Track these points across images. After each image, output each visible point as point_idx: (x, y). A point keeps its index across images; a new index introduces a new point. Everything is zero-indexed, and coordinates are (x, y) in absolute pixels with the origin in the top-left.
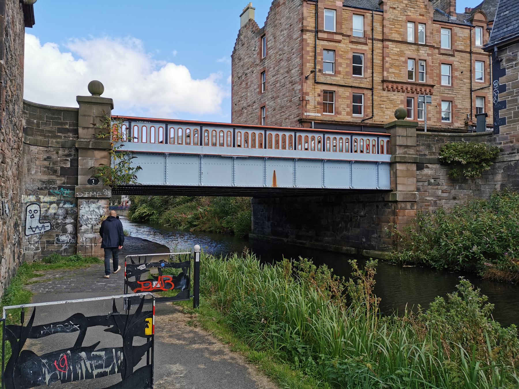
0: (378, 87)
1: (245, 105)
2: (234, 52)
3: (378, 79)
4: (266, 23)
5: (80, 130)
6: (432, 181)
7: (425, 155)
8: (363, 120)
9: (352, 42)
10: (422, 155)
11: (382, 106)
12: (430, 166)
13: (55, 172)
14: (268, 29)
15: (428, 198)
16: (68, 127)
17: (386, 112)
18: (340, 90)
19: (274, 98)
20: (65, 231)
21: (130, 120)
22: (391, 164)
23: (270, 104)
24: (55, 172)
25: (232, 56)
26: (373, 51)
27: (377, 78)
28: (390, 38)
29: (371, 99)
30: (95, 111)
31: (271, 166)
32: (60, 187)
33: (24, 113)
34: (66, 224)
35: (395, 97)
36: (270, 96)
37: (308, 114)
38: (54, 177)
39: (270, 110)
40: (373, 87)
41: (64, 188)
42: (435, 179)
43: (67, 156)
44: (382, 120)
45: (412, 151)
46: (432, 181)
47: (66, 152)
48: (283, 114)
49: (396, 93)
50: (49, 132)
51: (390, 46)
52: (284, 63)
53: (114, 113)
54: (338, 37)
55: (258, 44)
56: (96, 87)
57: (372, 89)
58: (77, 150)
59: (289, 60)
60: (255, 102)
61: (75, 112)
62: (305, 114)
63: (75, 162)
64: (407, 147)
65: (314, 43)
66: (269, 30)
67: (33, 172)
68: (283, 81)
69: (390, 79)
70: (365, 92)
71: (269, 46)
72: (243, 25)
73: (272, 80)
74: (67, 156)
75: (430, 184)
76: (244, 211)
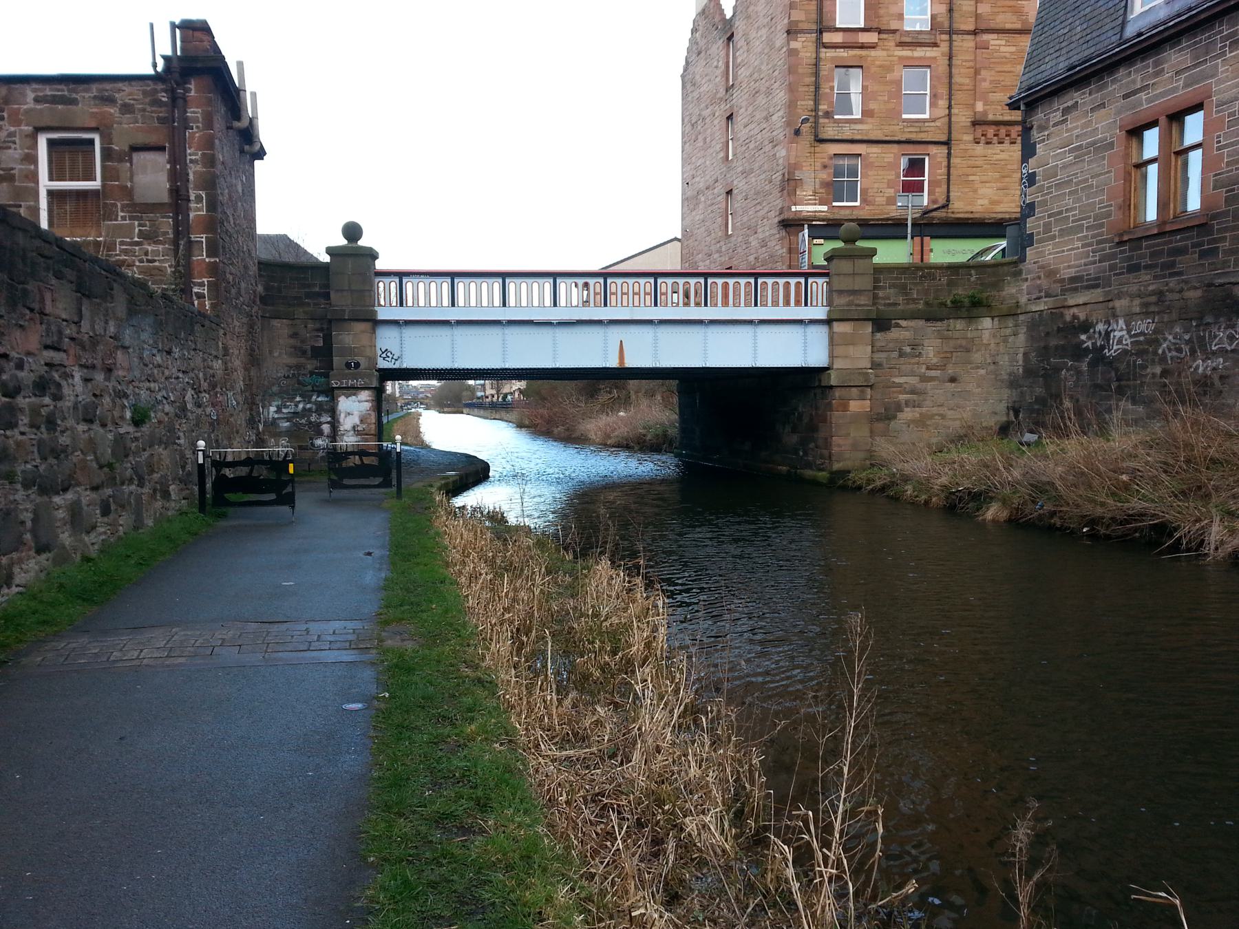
0: (964, 138)
1: (701, 185)
2: (685, 70)
3: (964, 119)
4: (735, 8)
5: (332, 295)
6: (908, 349)
7: (895, 304)
8: (925, 213)
9: (901, 44)
10: (890, 305)
11: (971, 178)
12: (903, 323)
13: (304, 353)
14: (737, 23)
15: (897, 380)
16: (317, 289)
17: (981, 191)
18: (875, 149)
19: (746, 173)
20: (320, 433)
21: (401, 275)
22: (828, 322)
23: (740, 185)
24: (304, 353)
25: (683, 76)
26: (950, 58)
27: (962, 117)
28: (993, 26)
29: (945, 163)
30: (350, 263)
31: (616, 334)
32: (312, 373)
33: (260, 276)
34: (321, 423)
35: (1003, 156)
36: (740, 169)
37: (799, 208)
38: (302, 360)
39: (739, 198)
40: (949, 139)
41: (317, 374)
42: (914, 346)
43: (317, 330)
44: (969, 208)
45: (863, 300)
46: (908, 349)
47: (318, 326)
48: (759, 207)
49: (1006, 146)
50: (296, 298)
51: (992, 42)
52: (761, 100)
53: (380, 265)
54: (872, 38)
55: (723, 53)
56: (352, 231)
57: (947, 143)
58: (330, 321)
59: (769, 92)
60: (716, 181)
61: (324, 267)
62: (793, 208)
63: (328, 339)
64: (853, 292)
65: (814, 55)
66: (740, 27)
67: (276, 354)
68: (759, 136)
69: (991, 117)
70: (933, 150)
71: (739, 60)
72: (700, 9)
73: (743, 134)
74: (317, 330)
75: (902, 354)
76: (656, 412)
